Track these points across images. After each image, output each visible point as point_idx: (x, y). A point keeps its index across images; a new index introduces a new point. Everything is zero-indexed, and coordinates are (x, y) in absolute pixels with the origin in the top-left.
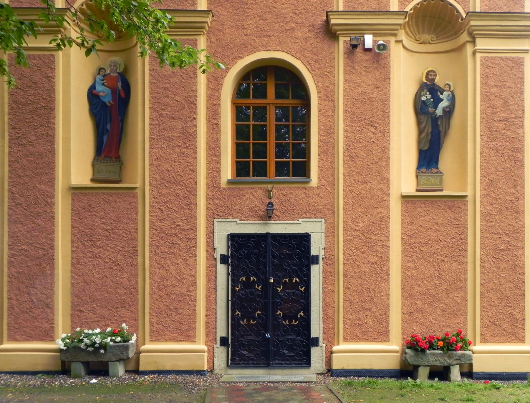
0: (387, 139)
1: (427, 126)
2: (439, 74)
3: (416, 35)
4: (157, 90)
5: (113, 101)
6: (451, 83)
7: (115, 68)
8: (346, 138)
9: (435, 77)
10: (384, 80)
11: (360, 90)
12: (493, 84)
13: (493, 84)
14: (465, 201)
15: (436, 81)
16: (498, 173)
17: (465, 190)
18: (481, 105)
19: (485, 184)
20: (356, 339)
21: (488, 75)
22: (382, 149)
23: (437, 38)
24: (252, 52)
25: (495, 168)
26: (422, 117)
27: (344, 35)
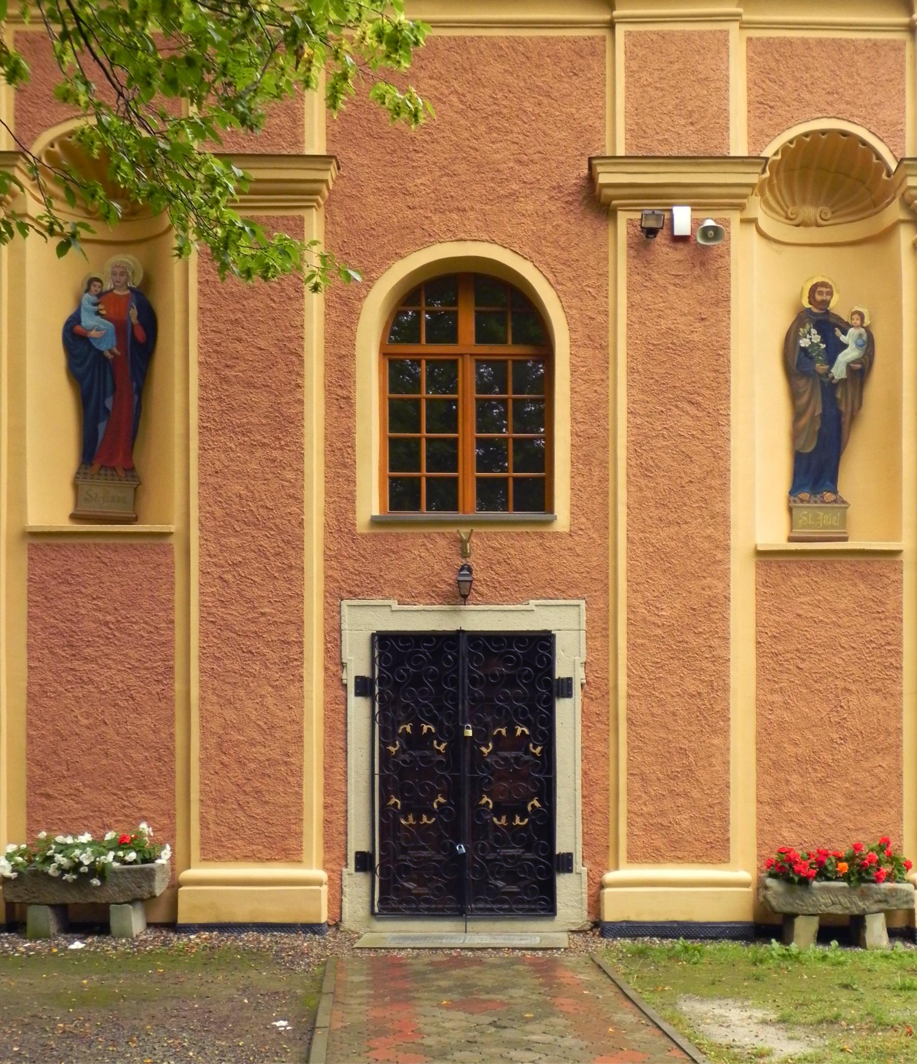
0: (724, 429)
1: (812, 402)
2: (838, 292)
4: (215, 324)
5: (118, 347)
6: (865, 311)
7: (123, 278)
8: (633, 427)
9: (828, 297)
10: (717, 304)
11: (664, 324)
14: (897, 562)
15: (832, 304)
17: (897, 538)
20: (655, 856)
22: (712, 451)
23: (833, 213)
24: (424, 245)
26: (802, 383)
27: (628, 208)
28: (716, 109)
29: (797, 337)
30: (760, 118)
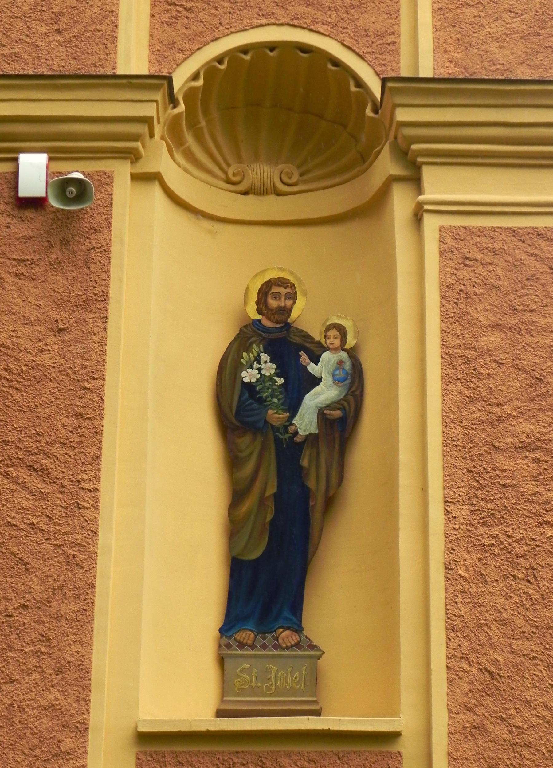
0: (88, 514)
1: (261, 473)
2: (305, 294)
3: (229, 165)
6: (347, 324)
9: (289, 303)
10: (85, 305)
12: (485, 318)
13: (485, 318)
14: (390, 755)
15: (294, 314)
16: (516, 644)
17: (394, 712)
18: (445, 392)
19: (466, 687)
21: (470, 289)
22: (64, 552)
23: (301, 175)
25: (503, 622)
26: (244, 441)
28: (97, 10)
29: (238, 367)
30: (169, 25)
